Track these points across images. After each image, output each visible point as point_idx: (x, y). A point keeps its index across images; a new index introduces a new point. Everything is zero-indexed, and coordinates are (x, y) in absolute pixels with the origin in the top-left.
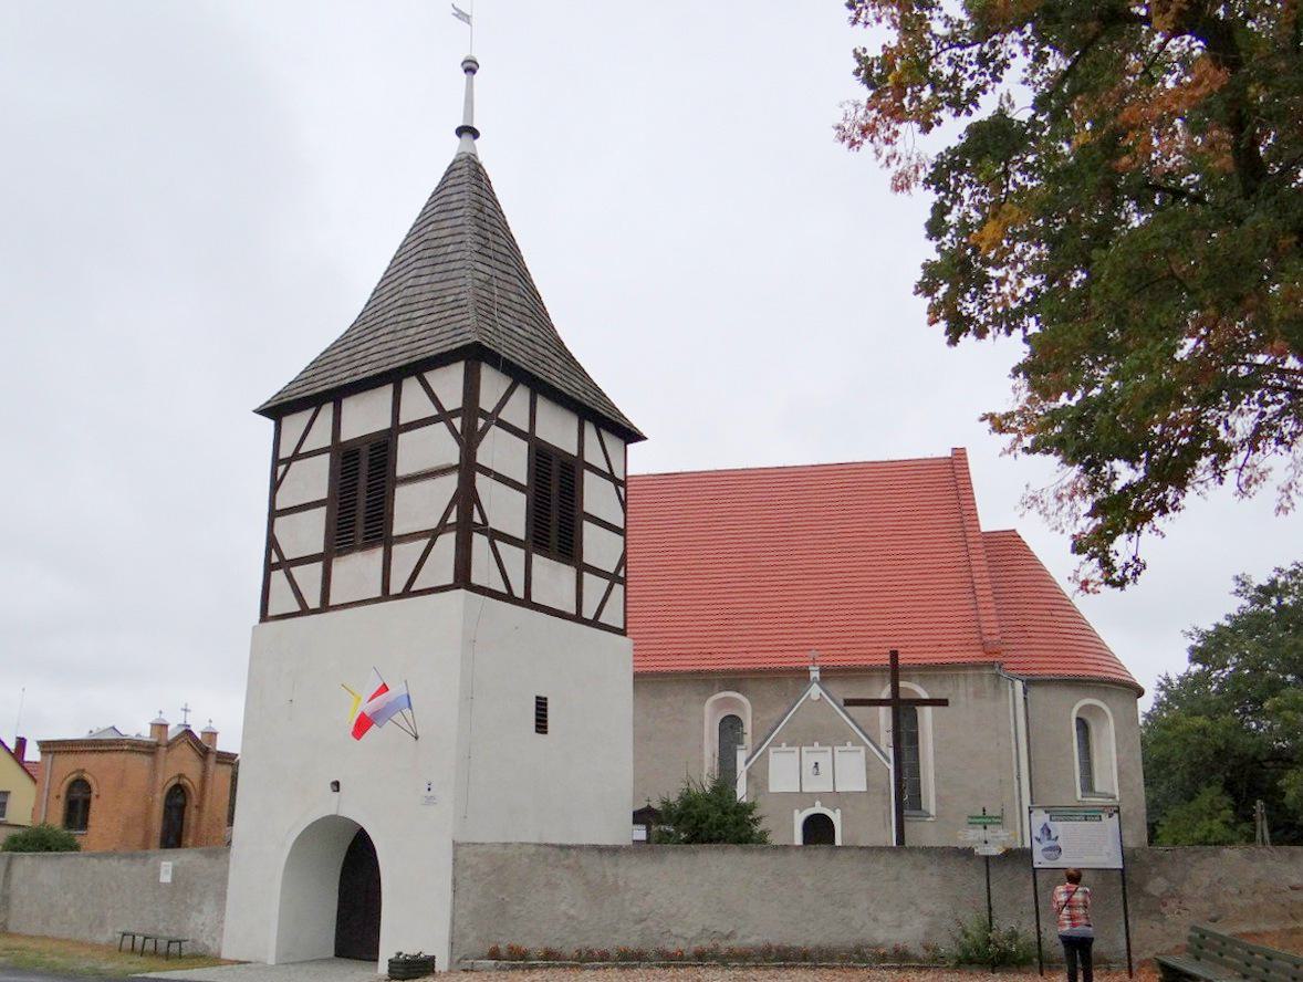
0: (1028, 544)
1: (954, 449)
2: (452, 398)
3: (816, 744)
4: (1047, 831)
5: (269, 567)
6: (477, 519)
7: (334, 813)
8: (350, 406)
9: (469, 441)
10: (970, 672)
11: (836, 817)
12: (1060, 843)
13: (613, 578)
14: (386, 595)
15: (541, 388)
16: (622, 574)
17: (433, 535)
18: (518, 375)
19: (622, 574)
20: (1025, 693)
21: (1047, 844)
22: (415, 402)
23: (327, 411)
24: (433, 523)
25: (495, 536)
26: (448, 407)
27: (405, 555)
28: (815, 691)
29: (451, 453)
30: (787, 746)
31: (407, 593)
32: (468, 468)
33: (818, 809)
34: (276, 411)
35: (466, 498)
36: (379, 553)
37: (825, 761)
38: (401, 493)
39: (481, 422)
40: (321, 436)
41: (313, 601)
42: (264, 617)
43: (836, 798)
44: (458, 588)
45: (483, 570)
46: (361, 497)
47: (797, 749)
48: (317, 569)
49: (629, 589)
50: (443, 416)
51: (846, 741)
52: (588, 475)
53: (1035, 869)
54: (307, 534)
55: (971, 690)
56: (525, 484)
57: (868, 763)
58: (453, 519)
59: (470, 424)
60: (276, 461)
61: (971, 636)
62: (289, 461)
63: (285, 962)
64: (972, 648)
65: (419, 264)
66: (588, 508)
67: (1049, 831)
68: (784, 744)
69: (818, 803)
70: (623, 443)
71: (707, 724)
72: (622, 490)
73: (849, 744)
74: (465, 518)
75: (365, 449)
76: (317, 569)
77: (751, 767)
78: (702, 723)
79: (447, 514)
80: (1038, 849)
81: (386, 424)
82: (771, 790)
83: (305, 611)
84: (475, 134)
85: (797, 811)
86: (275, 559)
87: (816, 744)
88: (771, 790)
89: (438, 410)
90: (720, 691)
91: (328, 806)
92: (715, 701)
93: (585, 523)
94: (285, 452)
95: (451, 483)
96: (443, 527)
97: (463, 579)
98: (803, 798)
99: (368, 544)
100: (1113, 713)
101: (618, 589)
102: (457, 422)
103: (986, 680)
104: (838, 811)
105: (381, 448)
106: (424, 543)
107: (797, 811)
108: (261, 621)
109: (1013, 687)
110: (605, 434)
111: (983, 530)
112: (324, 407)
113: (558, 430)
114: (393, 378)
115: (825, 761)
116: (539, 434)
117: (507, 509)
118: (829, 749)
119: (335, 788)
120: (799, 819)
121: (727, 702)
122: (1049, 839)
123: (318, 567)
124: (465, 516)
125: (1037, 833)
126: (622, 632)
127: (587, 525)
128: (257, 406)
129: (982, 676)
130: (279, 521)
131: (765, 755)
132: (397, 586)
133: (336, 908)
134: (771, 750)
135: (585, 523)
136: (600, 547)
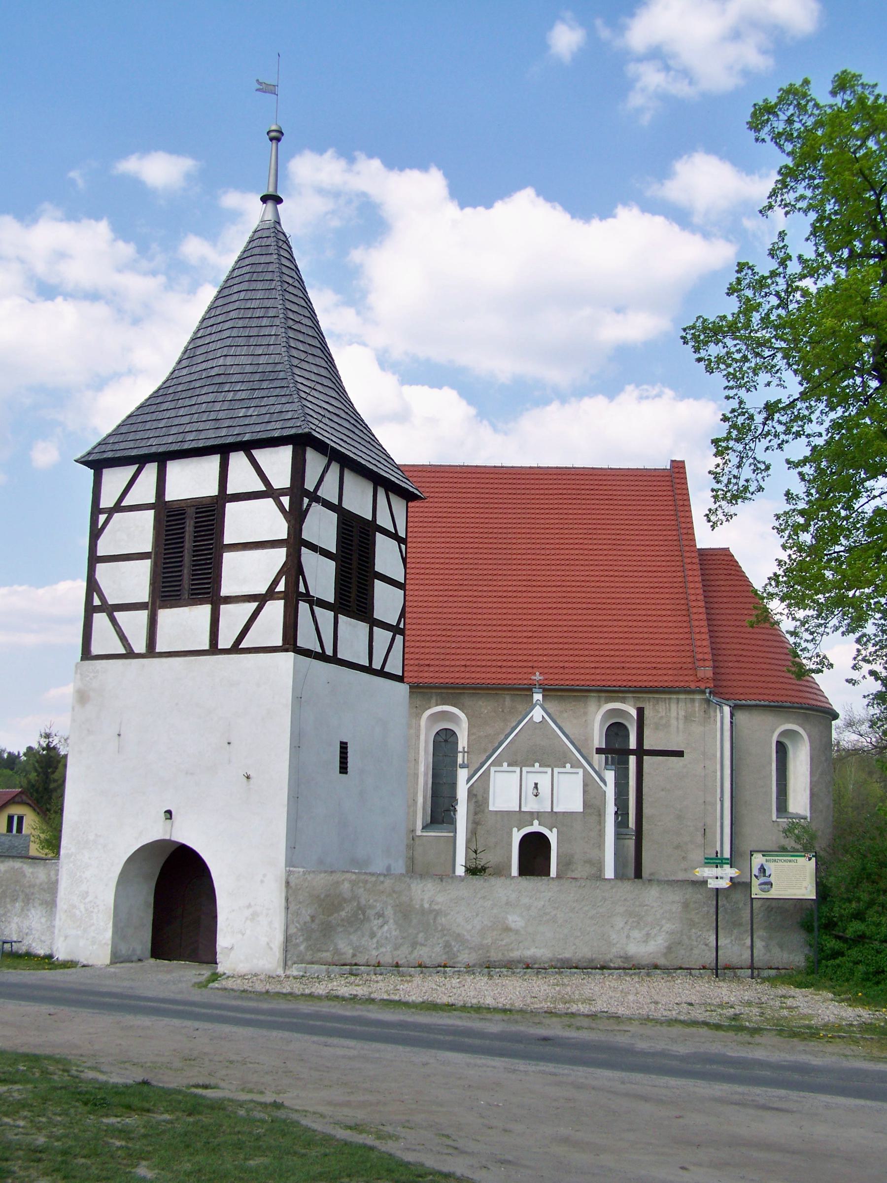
0: (740, 564)
1: (672, 461)
2: (281, 479)
3: (537, 765)
4: (762, 869)
5: (90, 610)
6: (302, 589)
7: (168, 838)
8: (174, 468)
9: (296, 517)
10: (682, 696)
11: (553, 837)
12: (772, 879)
13: (396, 630)
14: (214, 649)
15: (347, 463)
16: (402, 626)
17: (261, 600)
18: (334, 456)
19: (402, 626)
20: (732, 718)
21: (763, 879)
22: (242, 474)
23: (150, 472)
24: (262, 589)
25: (315, 603)
26: (276, 485)
27: (233, 617)
28: (537, 714)
29: (280, 529)
30: (508, 766)
31: (236, 649)
32: (295, 543)
33: (536, 827)
34: (98, 463)
35: (293, 569)
36: (207, 609)
37: (544, 781)
38: (229, 559)
39: (306, 501)
40: (145, 489)
41: (140, 646)
42: (87, 654)
43: (554, 818)
44: (287, 650)
45: (306, 638)
46: (188, 554)
47: (518, 769)
48: (143, 616)
49: (407, 638)
50: (270, 492)
51: (565, 763)
52: (379, 537)
53: (752, 899)
54: (132, 582)
55: (682, 713)
56: (376, 580)
57: (585, 785)
58: (281, 587)
59: (298, 501)
60: (96, 510)
61: (684, 660)
62: (111, 512)
63: (117, 958)
64: (686, 672)
65: (235, 333)
66: (378, 568)
67: (765, 870)
68: (505, 764)
69: (536, 822)
70: (405, 502)
71: (422, 737)
72: (403, 547)
73: (568, 765)
74: (292, 588)
75: (191, 511)
76: (143, 616)
77: (472, 785)
78: (418, 737)
79: (275, 582)
80: (755, 882)
81: (214, 491)
82: (491, 808)
83: (130, 654)
84: (278, 200)
85: (515, 830)
86: (97, 602)
87: (537, 765)
88: (491, 808)
89: (265, 486)
90: (437, 705)
91: (156, 831)
92: (432, 715)
93: (334, 550)
94: (107, 502)
95: (280, 556)
96: (270, 594)
97: (290, 642)
98: (522, 817)
99: (195, 599)
100: (809, 737)
101: (399, 638)
102: (286, 501)
103: (697, 705)
104: (555, 830)
105: (209, 514)
106: (254, 605)
107: (515, 830)
108: (82, 660)
109: (722, 712)
110: (391, 495)
111: (698, 547)
112: (148, 465)
113: (359, 499)
114: (224, 451)
115: (544, 781)
116: (345, 505)
117: (322, 577)
118: (549, 770)
119: (169, 816)
120: (517, 836)
121: (444, 715)
122: (765, 876)
123: (144, 615)
124: (292, 585)
125: (755, 871)
126: (400, 679)
127: (378, 584)
128: (78, 456)
129: (693, 700)
130: (100, 567)
131: (487, 773)
132: (225, 642)
133: (152, 918)
134: (493, 769)
135: (334, 550)
136: (387, 602)
